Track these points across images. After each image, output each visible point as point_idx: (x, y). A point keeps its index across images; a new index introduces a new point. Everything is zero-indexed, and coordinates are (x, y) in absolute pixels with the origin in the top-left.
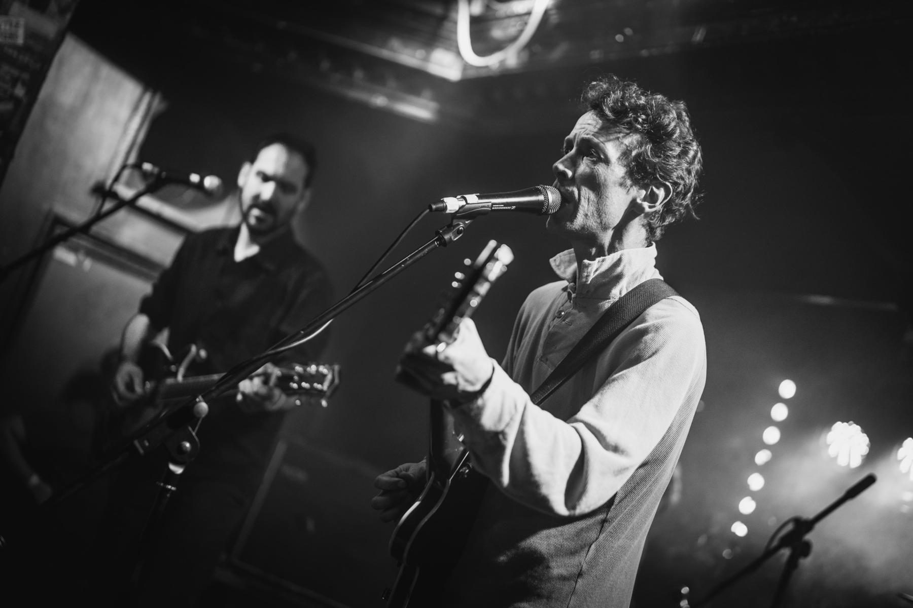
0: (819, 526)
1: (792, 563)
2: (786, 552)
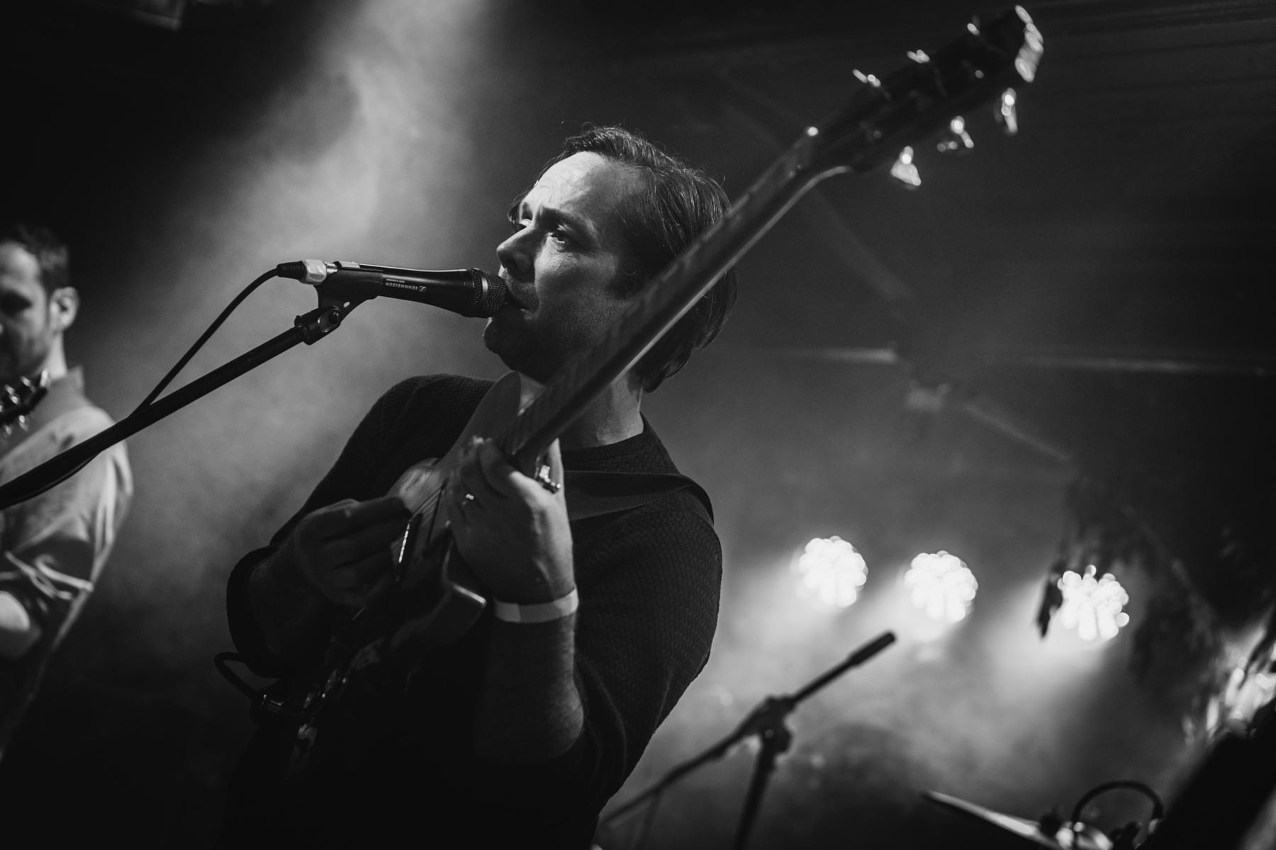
0: (802, 707)
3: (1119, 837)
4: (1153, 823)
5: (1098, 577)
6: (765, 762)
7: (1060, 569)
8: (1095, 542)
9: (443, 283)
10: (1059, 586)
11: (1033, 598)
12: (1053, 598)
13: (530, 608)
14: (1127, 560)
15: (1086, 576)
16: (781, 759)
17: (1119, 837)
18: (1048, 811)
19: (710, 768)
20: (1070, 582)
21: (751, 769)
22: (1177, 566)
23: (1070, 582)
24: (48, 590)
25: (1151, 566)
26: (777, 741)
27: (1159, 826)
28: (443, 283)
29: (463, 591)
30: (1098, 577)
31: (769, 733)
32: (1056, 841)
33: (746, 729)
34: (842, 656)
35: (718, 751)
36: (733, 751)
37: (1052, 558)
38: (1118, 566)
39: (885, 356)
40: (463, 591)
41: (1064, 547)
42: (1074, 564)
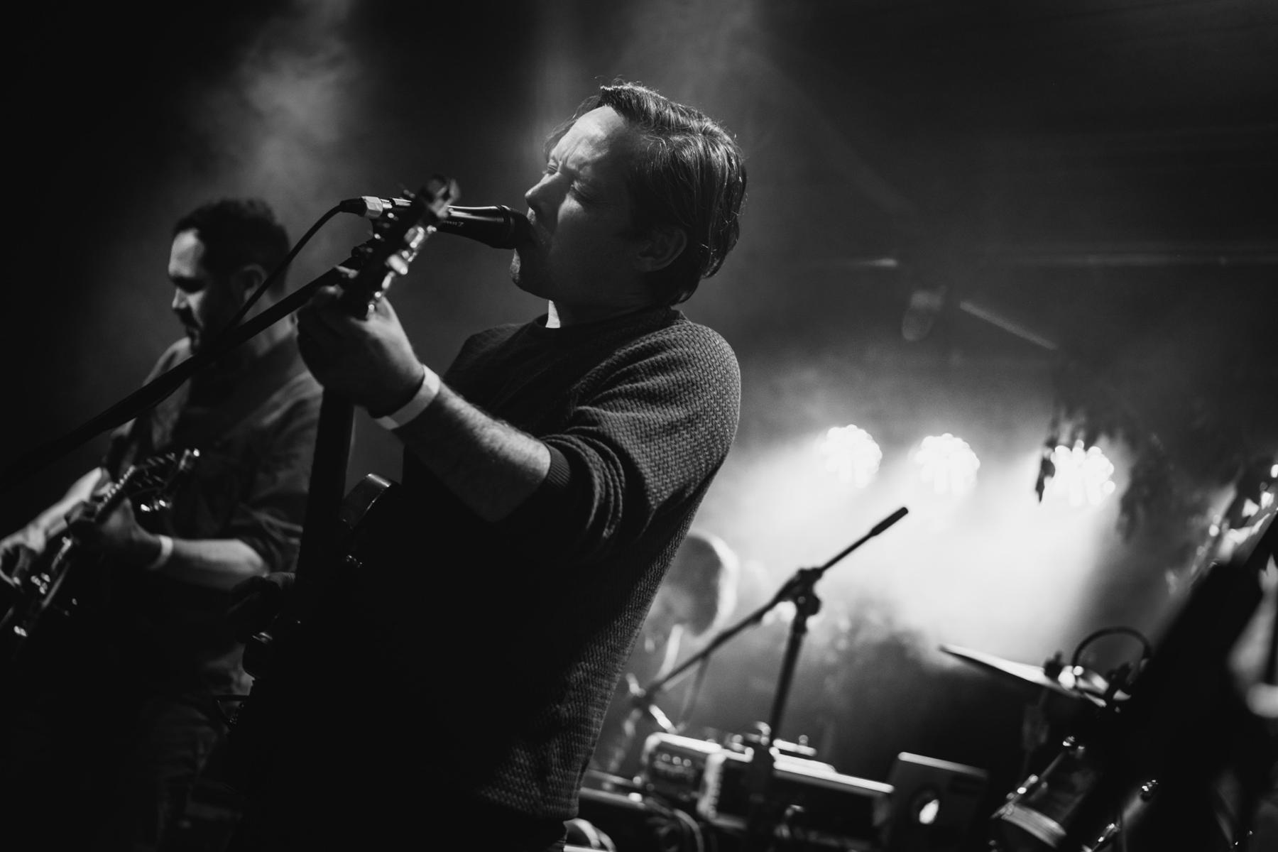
0: (828, 574)
1: (799, 628)
2: (787, 611)
3: (1114, 676)
4: (1144, 662)
5: (1086, 448)
6: (799, 628)
7: (1052, 444)
8: (1082, 419)
9: (621, 353)
10: (1053, 460)
11: (1031, 468)
12: (1047, 468)
13: (399, 413)
14: (1111, 435)
15: (1075, 449)
16: (812, 622)
17: (1114, 676)
18: (1051, 656)
19: (749, 634)
20: (1060, 456)
21: (787, 632)
22: (1155, 438)
23: (1060, 456)
24: (278, 536)
25: (1133, 441)
26: (809, 605)
27: (1147, 665)
28: (621, 353)
29: (592, 518)
30: (1086, 448)
31: (801, 600)
32: (1058, 683)
33: (782, 596)
34: (865, 531)
35: (757, 617)
36: (768, 618)
37: (1044, 437)
38: (1103, 441)
39: (889, 263)
40: (592, 518)
41: (1055, 424)
42: (1064, 438)
